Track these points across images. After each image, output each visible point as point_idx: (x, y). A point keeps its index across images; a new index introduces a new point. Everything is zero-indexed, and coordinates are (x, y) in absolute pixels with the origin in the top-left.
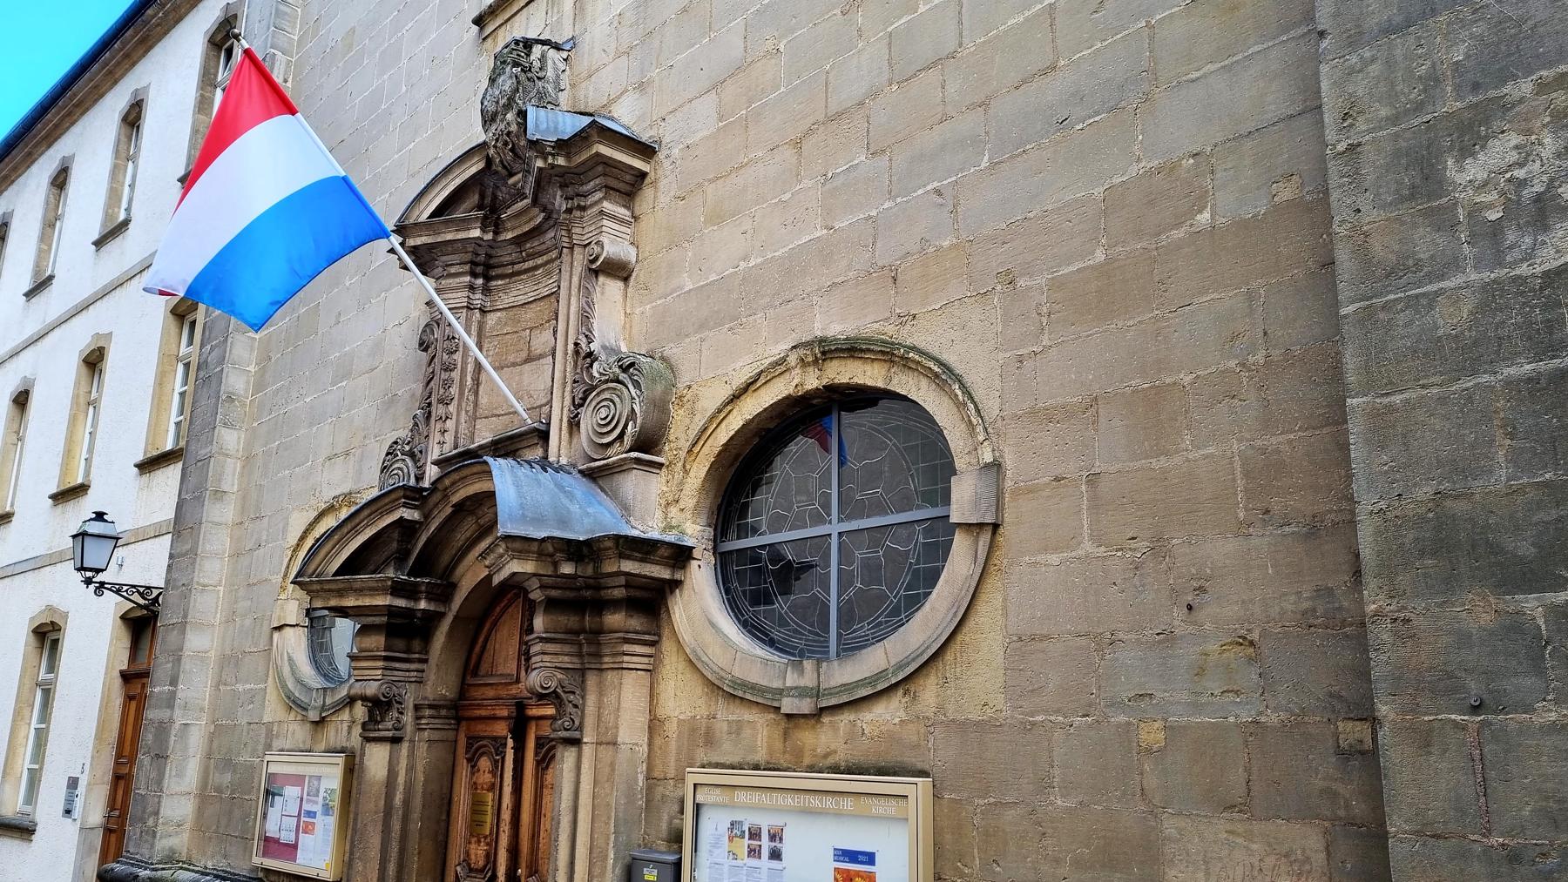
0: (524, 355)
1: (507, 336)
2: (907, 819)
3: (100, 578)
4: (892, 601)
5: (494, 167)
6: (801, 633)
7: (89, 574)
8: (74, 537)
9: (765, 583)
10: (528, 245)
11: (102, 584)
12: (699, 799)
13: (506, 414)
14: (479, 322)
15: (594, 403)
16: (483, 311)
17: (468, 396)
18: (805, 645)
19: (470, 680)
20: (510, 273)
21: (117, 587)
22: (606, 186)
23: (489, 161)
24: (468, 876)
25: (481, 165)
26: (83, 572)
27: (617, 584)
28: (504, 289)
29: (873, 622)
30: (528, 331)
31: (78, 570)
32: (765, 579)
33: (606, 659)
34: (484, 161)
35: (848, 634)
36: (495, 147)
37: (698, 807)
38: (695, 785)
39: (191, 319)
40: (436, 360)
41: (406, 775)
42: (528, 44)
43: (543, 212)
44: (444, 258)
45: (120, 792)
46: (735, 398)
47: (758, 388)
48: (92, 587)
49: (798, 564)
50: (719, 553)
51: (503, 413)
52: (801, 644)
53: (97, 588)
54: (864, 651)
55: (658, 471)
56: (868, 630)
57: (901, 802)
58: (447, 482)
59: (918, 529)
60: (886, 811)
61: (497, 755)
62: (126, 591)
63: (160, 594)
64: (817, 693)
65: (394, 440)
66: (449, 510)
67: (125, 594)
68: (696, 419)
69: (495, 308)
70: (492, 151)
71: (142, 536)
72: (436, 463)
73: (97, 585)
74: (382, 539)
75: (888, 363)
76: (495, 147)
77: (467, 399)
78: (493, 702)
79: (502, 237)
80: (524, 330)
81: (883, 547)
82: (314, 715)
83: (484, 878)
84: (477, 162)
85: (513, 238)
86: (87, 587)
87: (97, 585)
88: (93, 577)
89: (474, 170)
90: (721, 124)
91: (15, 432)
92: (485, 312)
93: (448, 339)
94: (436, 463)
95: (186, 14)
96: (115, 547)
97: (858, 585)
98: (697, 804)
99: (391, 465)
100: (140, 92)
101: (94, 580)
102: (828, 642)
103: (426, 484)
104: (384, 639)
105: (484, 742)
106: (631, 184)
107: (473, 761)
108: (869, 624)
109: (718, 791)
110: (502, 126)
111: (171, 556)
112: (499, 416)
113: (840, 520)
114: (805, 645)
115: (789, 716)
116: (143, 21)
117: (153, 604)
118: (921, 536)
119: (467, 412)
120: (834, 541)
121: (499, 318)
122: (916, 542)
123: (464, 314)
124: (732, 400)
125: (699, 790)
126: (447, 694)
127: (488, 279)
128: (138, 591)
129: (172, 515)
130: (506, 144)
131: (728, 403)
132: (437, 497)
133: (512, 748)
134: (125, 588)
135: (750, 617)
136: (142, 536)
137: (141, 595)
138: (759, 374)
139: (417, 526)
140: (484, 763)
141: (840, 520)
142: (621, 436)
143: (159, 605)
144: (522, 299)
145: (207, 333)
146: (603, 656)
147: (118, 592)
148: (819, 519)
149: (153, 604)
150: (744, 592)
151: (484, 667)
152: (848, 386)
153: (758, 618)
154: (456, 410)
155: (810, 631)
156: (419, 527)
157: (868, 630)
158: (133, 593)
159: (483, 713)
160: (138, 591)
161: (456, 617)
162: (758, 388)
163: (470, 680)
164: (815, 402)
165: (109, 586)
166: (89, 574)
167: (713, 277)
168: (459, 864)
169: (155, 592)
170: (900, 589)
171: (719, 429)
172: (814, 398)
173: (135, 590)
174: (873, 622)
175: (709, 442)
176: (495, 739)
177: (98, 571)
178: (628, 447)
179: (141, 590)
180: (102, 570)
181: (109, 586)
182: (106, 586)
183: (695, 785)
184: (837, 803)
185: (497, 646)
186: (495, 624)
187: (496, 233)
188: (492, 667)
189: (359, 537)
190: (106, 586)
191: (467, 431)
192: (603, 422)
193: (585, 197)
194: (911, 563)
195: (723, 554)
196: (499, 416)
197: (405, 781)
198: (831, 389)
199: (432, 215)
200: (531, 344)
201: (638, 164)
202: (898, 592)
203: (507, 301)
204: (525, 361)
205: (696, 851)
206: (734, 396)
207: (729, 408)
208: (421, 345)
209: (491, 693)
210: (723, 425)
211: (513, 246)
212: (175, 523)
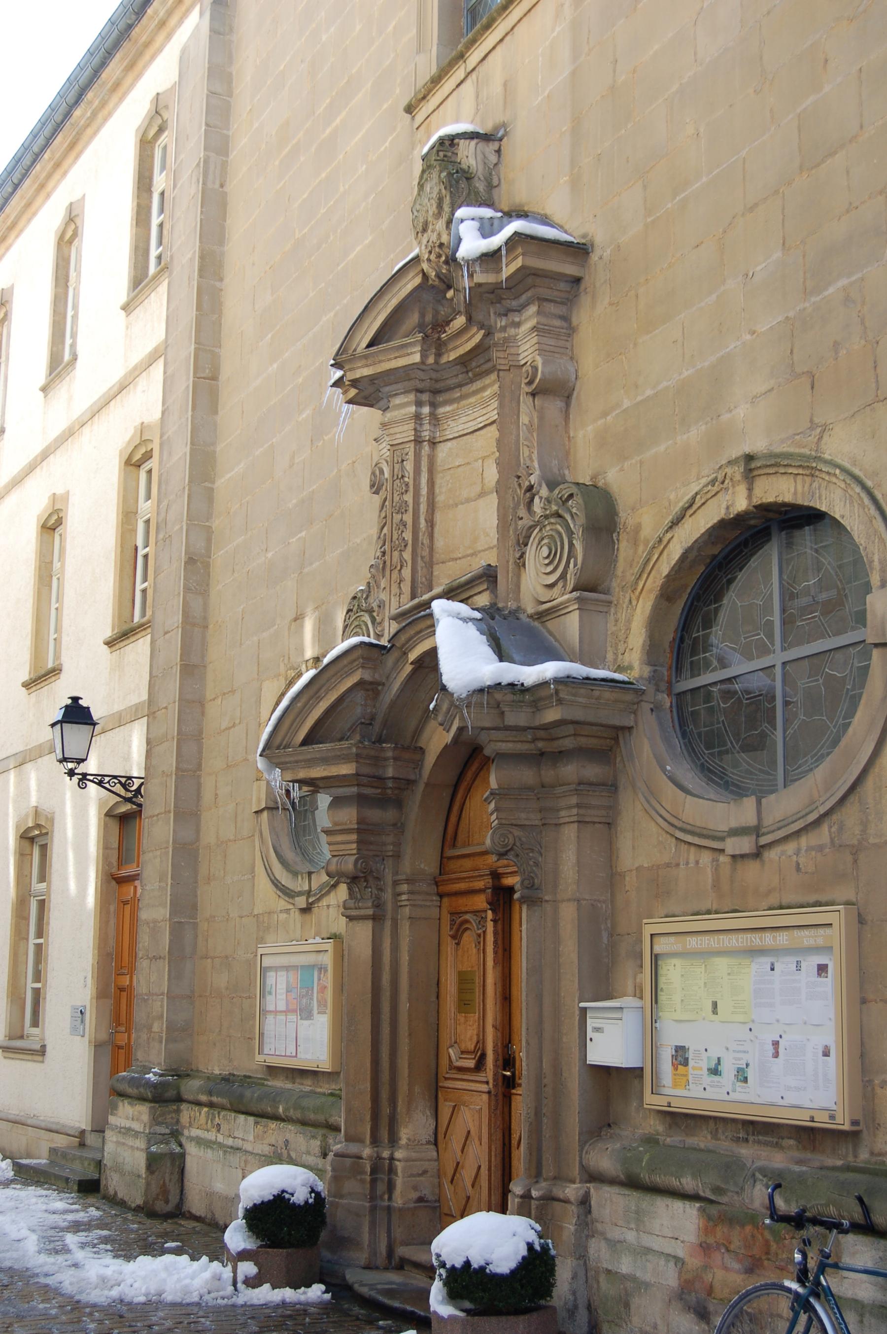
0: (478, 489)
1: (460, 469)
2: (832, 947)
3: (81, 769)
4: (832, 731)
5: (430, 282)
6: (751, 773)
7: (71, 765)
8: (53, 725)
9: (718, 723)
10: (474, 364)
11: (84, 776)
12: (657, 949)
13: (464, 557)
14: (429, 456)
15: (537, 541)
16: (433, 443)
17: (422, 540)
18: (757, 785)
19: (449, 853)
20: (458, 397)
21: (99, 778)
22: (539, 299)
23: (425, 276)
24: (460, 1058)
25: (418, 280)
26: (65, 763)
27: (567, 734)
28: (453, 416)
29: (816, 755)
30: (480, 461)
31: (61, 761)
32: (718, 719)
33: (563, 813)
34: (421, 275)
35: (796, 769)
36: (429, 260)
37: (656, 958)
38: (652, 935)
39: (148, 468)
40: (387, 503)
41: (391, 954)
42: (449, 143)
43: (481, 328)
44: (387, 389)
45: (124, 1001)
46: (676, 522)
47: (695, 512)
48: (75, 779)
49: (747, 699)
50: (675, 695)
51: (460, 555)
52: (753, 784)
53: (80, 780)
54: (797, 783)
55: (605, 609)
56: (812, 764)
57: (828, 931)
58: (403, 638)
59: (852, 652)
60: (815, 941)
61: (478, 929)
62: (109, 782)
63: (142, 784)
64: (756, 831)
65: (352, 595)
66: (409, 668)
67: (107, 785)
68: (641, 548)
69: (445, 438)
70: (425, 266)
71: (121, 720)
72: (395, 618)
73: (80, 777)
74: (345, 704)
75: (810, 478)
76: (429, 260)
77: (422, 544)
78: (471, 874)
79: (444, 359)
80: (476, 460)
81: (822, 675)
82: (301, 902)
83: (474, 1058)
84: (413, 277)
85: (456, 359)
86: (71, 779)
87: (80, 777)
88: (76, 768)
89: (410, 287)
90: (649, 220)
91: (428, 1143)
92: (434, 443)
93: (397, 478)
94: (395, 618)
95: (41, 546)
96: (92, 737)
97: (802, 717)
98: (656, 956)
99: (351, 624)
100: (74, 206)
101: (76, 771)
102: (776, 780)
103: (384, 642)
104: (356, 811)
105: (467, 917)
106: (567, 291)
107: (456, 937)
108: (812, 758)
109: (672, 939)
110: (434, 237)
111: (148, 742)
112: (456, 559)
113: (784, 649)
114: (757, 785)
115: (734, 857)
116: (72, 125)
117: (135, 796)
118: (856, 661)
119: (422, 558)
120: (778, 670)
121: (450, 449)
122: (852, 667)
123: (412, 449)
124: (671, 527)
125: (656, 939)
126: (426, 868)
127: (434, 405)
128: (120, 782)
129: (145, 697)
130: (439, 256)
131: (667, 531)
132: (395, 654)
133: (491, 920)
134: (107, 779)
135: (706, 761)
136: (121, 720)
137: (124, 786)
138: (694, 499)
139: (380, 688)
140: (468, 938)
141: (784, 649)
142: (563, 576)
143: (142, 797)
144: (472, 426)
145: (163, 487)
146: (558, 810)
147: (100, 783)
148: (765, 651)
149: (135, 796)
150: (699, 734)
151: (461, 837)
152: (775, 504)
153: (713, 762)
154: (410, 557)
155: (761, 771)
156: (382, 689)
157: (812, 764)
158: (115, 784)
159: (462, 886)
160: (120, 782)
161: (427, 785)
162: (695, 512)
163: (449, 853)
164: (752, 522)
165: (91, 778)
166: (71, 765)
167: (649, 392)
168: (451, 1046)
169: (137, 783)
170: (839, 717)
171: (661, 558)
172: (751, 518)
173: (116, 781)
174: (816, 755)
175: (651, 575)
176: (475, 912)
177: (80, 761)
178: (572, 586)
179: (123, 780)
180: (83, 760)
181: (91, 778)
182: (88, 777)
183: (652, 935)
184: (774, 938)
185: (471, 814)
186: (469, 790)
187: (439, 355)
188: (469, 836)
189: (321, 704)
190: (88, 777)
191: (424, 579)
192: (547, 561)
193: (519, 311)
194: (848, 689)
195: (679, 695)
196: (456, 559)
197: (391, 961)
198: (764, 509)
199: (370, 345)
200: (484, 476)
201: (569, 269)
202: (837, 722)
203: (456, 429)
204: (479, 496)
205: (656, 1002)
206: (672, 522)
207: (669, 535)
208: (372, 486)
209: (467, 863)
210: (665, 553)
211: (458, 367)
212: (149, 705)
